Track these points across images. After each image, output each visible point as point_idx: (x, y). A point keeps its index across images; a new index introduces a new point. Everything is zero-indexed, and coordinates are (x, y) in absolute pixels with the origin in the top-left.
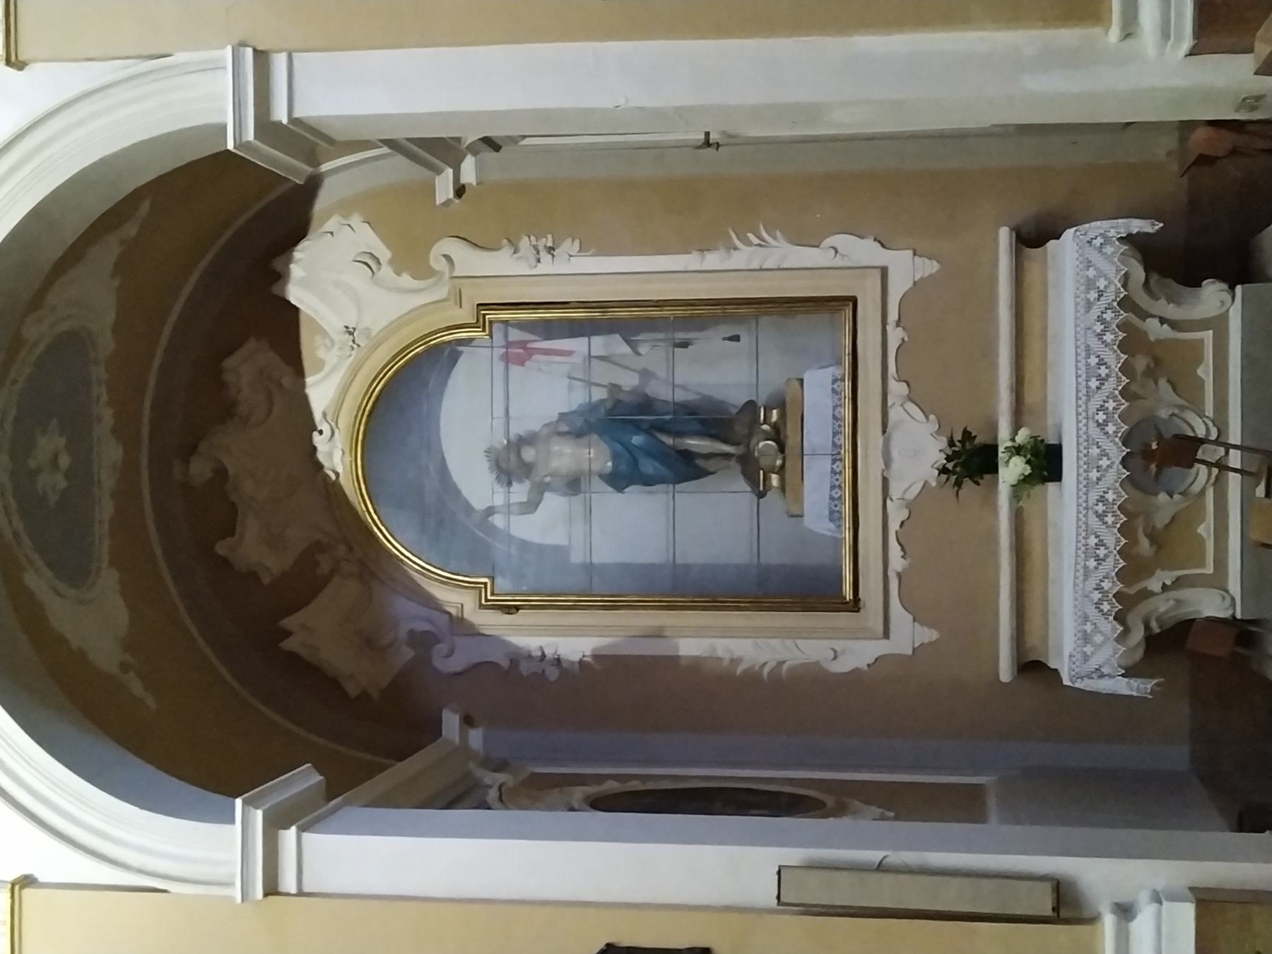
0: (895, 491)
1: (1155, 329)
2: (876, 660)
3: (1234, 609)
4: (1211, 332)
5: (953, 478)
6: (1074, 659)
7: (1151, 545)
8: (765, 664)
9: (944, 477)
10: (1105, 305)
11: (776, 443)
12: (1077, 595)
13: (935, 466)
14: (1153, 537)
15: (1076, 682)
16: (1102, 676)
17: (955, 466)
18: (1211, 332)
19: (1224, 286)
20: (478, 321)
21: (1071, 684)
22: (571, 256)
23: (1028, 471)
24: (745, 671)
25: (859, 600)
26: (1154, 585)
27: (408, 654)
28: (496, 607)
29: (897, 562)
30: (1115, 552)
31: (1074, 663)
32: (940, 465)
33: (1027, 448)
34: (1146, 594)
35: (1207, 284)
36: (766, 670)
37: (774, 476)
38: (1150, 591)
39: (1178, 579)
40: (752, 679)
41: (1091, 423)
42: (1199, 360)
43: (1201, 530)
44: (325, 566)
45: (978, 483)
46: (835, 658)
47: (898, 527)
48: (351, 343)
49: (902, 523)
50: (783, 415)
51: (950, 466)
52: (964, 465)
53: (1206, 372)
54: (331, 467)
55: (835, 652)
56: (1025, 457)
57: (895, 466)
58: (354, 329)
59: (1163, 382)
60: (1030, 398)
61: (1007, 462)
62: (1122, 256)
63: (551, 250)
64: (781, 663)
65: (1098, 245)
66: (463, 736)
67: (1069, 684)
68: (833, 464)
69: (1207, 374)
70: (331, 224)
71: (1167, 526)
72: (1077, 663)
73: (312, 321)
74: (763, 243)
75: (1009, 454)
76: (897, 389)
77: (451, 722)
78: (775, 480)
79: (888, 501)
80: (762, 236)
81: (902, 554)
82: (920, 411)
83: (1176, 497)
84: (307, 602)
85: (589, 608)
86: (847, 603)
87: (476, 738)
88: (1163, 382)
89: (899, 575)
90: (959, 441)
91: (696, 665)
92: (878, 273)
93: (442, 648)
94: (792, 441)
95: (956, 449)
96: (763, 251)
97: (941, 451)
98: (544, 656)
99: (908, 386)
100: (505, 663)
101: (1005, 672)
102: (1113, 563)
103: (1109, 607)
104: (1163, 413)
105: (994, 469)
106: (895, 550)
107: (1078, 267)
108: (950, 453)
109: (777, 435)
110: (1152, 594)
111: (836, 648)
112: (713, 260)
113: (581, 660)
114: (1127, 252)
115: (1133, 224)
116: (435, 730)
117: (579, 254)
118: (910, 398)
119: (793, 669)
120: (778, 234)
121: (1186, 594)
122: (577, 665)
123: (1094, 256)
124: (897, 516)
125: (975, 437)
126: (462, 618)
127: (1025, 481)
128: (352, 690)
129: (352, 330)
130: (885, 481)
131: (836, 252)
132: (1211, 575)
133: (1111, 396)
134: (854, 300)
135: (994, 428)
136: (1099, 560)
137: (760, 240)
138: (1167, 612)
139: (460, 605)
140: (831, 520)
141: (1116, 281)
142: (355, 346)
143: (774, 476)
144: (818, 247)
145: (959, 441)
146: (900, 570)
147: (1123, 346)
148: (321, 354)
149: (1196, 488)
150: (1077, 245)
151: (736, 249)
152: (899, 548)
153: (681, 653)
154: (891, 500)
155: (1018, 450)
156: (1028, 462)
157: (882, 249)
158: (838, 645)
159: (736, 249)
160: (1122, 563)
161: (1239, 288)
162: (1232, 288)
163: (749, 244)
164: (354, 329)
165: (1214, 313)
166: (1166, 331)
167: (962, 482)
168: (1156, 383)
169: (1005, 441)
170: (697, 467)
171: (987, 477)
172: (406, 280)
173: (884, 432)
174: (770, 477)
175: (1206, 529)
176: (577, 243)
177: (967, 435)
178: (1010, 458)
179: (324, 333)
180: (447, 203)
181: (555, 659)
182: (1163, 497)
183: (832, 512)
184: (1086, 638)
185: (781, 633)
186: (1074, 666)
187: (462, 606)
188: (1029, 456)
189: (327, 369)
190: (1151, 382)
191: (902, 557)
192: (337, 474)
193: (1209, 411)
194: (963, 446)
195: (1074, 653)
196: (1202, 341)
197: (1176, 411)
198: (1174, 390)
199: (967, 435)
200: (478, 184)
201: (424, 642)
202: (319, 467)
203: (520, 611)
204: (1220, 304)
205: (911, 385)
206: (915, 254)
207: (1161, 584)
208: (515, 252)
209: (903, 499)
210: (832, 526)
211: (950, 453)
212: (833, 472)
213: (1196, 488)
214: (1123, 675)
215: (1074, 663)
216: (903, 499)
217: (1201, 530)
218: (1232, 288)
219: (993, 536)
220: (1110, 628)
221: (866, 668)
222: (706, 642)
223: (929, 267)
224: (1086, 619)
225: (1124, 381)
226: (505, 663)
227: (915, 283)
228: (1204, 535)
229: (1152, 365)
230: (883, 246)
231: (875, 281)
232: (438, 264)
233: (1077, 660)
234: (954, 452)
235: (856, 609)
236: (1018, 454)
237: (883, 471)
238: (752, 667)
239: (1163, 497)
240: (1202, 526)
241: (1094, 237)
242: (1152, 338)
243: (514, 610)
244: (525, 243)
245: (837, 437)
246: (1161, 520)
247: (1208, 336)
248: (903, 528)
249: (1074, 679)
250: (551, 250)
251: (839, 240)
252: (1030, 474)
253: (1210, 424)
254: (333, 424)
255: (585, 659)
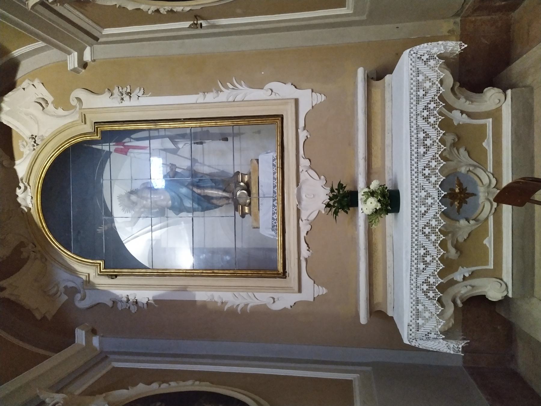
0: (304, 216)
1: (457, 117)
2: (295, 303)
3: (508, 292)
4: (491, 120)
5: (333, 209)
6: (411, 328)
7: (457, 252)
8: (238, 305)
9: (329, 209)
10: (430, 99)
11: (247, 191)
12: (412, 287)
13: (324, 203)
14: (457, 247)
15: (412, 342)
16: (428, 339)
17: (334, 203)
18: (491, 120)
19: (501, 91)
20: (94, 131)
21: (409, 344)
22: (139, 97)
23: (379, 206)
24: (229, 309)
25: (286, 272)
26: (458, 276)
27: (65, 298)
28: (105, 275)
29: (305, 253)
30: (437, 259)
31: (411, 330)
32: (326, 202)
33: (378, 193)
34: (453, 283)
35: (486, 91)
36: (239, 309)
37: (246, 208)
38: (456, 281)
39: (473, 272)
40: (232, 313)
41: (420, 175)
42: (483, 136)
43: (486, 242)
44: (25, 255)
45: (347, 213)
46: (274, 302)
47: (305, 235)
48: (33, 143)
49: (307, 232)
50: (250, 178)
51: (332, 203)
52: (339, 202)
53: (488, 144)
54: (26, 205)
55: (274, 299)
56: (377, 198)
57: (303, 203)
58: (36, 136)
59: (462, 150)
60: (376, 164)
61: (365, 201)
62: (440, 68)
63: (129, 94)
64: (247, 305)
65: (425, 60)
66: (89, 341)
67: (408, 343)
68: (273, 202)
69: (489, 146)
70: (24, 85)
71: (465, 240)
72: (413, 330)
73: (17, 133)
74: (237, 89)
75: (367, 196)
76: (304, 163)
77: (80, 335)
78: (247, 210)
79: (300, 221)
80: (236, 86)
81: (308, 248)
82: (317, 175)
83: (472, 222)
84: (12, 274)
85: (152, 275)
86: (280, 274)
87: (96, 341)
88: (462, 150)
89: (306, 260)
90: (336, 189)
91: (204, 305)
92: (293, 103)
93: (79, 296)
94: (254, 190)
95: (335, 194)
96: (235, 92)
97: (327, 195)
98: (128, 300)
99: (310, 161)
100: (110, 304)
101: (363, 319)
102: (435, 267)
103: (433, 295)
104: (463, 170)
105: (356, 204)
106: (304, 246)
107: (412, 74)
108: (331, 196)
109: (248, 188)
110: (457, 282)
111: (275, 297)
112: (210, 97)
113: (147, 302)
114: (443, 66)
115: (448, 44)
116: (71, 339)
117: (143, 96)
118: (311, 167)
119: (253, 307)
120: (242, 82)
121: (476, 282)
122: (145, 306)
123: (421, 66)
124: (305, 228)
125: (345, 187)
126: (89, 281)
127: (376, 212)
128: (38, 316)
129: (34, 137)
130: (298, 211)
131: (272, 91)
132: (492, 269)
133: (434, 158)
134: (282, 117)
135: (355, 182)
136: (426, 264)
137: (234, 86)
138: (466, 293)
139: (87, 275)
140: (273, 230)
141: (437, 83)
142: (35, 145)
143: (246, 208)
144: (263, 89)
145: (336, 189)
146: (307, 257)
147: (442, 125)
148: (22, 149)
149: (483, 216)
150: (411, 60)
151: (221, 91)
152: (306, 245)
153: (196, 299)
154: (302, 220)
155: (372, 194)
156: (379, 201)
157: (296, 89)
158: (275, 295)
159: (221, 91)
160: (442, 266)
161: (509, 92)
162: (504, 92)
163: (227, 88)
164: (36, 136)
165: (494, 107)
166: (464, 119)
167: (338, 212)
168: (458, 150)
169: (362, 189)
170: (213, 204)
171: (351, 208)
172: (60, 111)
173: (298, 185)
174: (245, 208)
175: (489, 242)
176: (142, 90)
177: (341, 186)
178: (367, 198)
179: (23, 139)
180: (74, 70)
181: (134, 302)
182: (463, 222)
183: (273, 226)
184: (418, 315)
185: (246, 289)
186: (411, 332)
187: (89, 274)
188: (379, 197)
189: (24, 156)
190: (455, 149)
191: (308, 250)
192: (29, 209)
193: (490, 168)
194: (339, 192)
195: (411, 323)
196: (484, 126)
197: (471, 168)
198: (469, 156)
199: (341, 186)
200: (92, 61)
201: (72, 292)
202: (19, 205)
203: (118, 277)
204: (498, 101)
205: (311, 161)
206: (312, 91)
207: (462, 277)
208: (112, 95)
209: (308, 220)
210: (273, 233)
211: (331, 196)
212: (274, 205)
213: (483, 216)
214: (443, 339)
215: (411, 330)
216: (308, 220)
217: (486, 242)
218: (504, 92)
219: (354, 241)
220: (433, 307)
221: (289, 308)
222: (209, 293)
223: (320, 98)
224: (418, 301)
225: (443, 148)
226: (110, 304)
227: (313, 107)
228: (488, 245)
229: (457, 140)
230: (296, 87)
231: (291, 108)
232: (74, 102)
233: (413, 328)
234: (333, 195)
235: (285, 277)
236: (373, 196)
237: (297, 205)
238: (233, 306)
239: (463, 222)
240: (487, 239)
241: (422, 54)
242: (456, 123)
243: (114, 277)
244: (116, 91)
245: (275, 188)
246: (462, 236)
247: (489, 122)
248: (307, 235)
249: (411, 340)
250: (129, 94)
251: (275, 85)
252: (380, 209)
253: (491, 176)
254: (26, 184)
255: (149, 301)
